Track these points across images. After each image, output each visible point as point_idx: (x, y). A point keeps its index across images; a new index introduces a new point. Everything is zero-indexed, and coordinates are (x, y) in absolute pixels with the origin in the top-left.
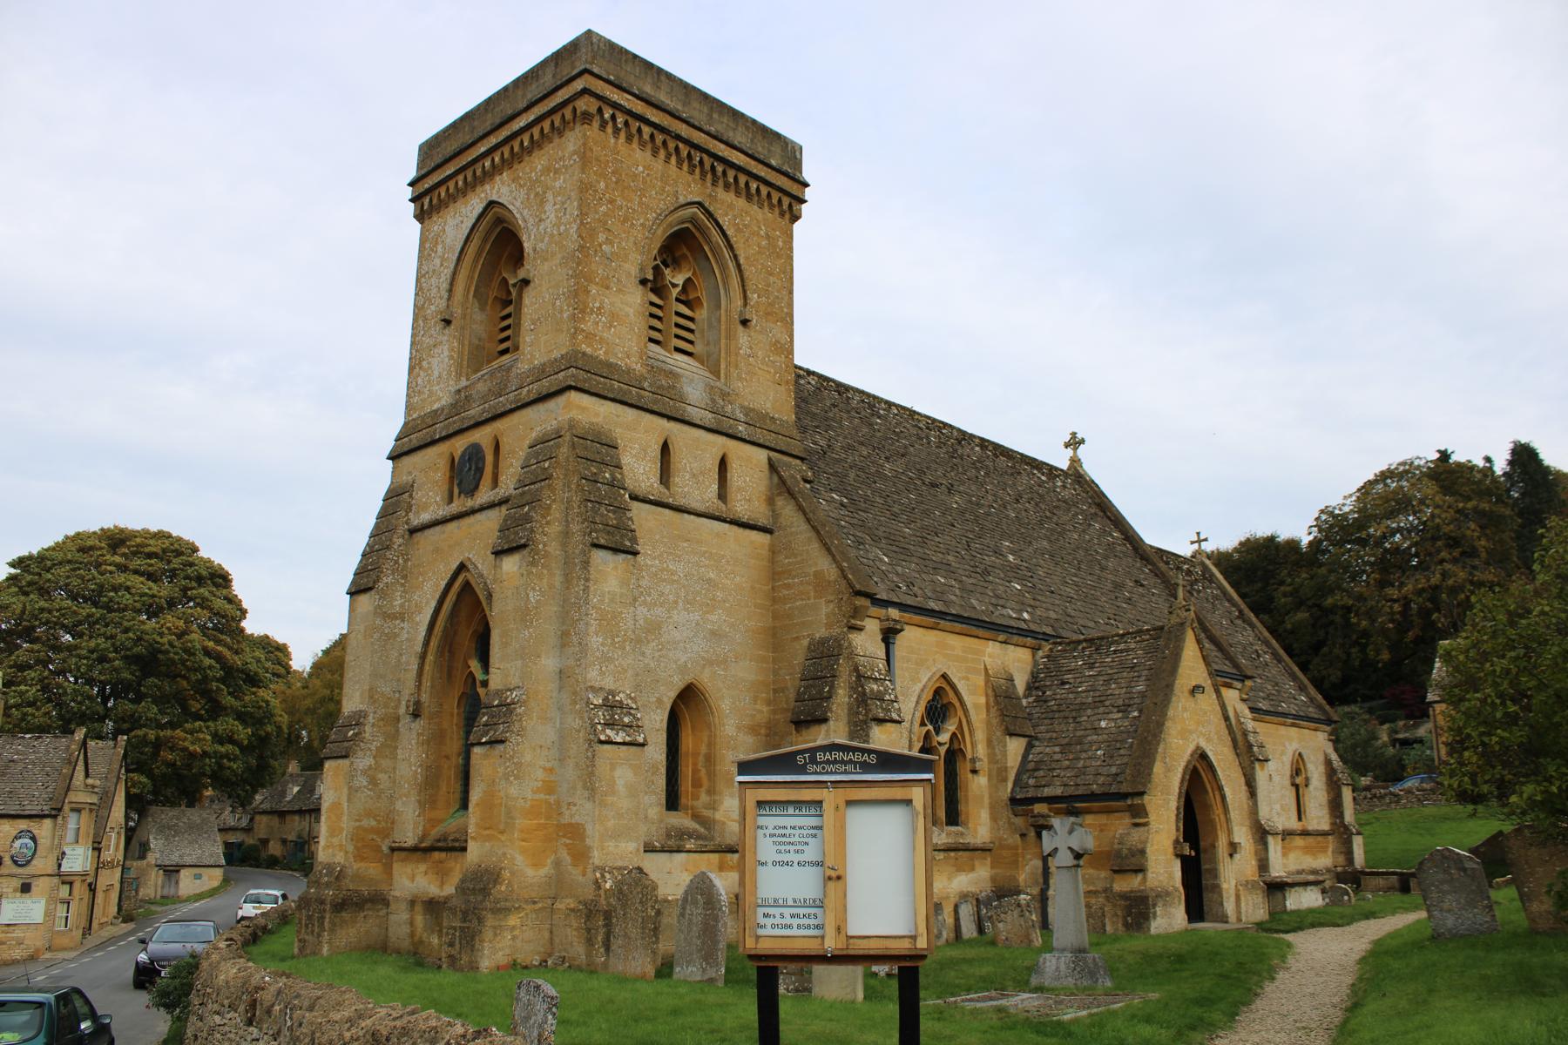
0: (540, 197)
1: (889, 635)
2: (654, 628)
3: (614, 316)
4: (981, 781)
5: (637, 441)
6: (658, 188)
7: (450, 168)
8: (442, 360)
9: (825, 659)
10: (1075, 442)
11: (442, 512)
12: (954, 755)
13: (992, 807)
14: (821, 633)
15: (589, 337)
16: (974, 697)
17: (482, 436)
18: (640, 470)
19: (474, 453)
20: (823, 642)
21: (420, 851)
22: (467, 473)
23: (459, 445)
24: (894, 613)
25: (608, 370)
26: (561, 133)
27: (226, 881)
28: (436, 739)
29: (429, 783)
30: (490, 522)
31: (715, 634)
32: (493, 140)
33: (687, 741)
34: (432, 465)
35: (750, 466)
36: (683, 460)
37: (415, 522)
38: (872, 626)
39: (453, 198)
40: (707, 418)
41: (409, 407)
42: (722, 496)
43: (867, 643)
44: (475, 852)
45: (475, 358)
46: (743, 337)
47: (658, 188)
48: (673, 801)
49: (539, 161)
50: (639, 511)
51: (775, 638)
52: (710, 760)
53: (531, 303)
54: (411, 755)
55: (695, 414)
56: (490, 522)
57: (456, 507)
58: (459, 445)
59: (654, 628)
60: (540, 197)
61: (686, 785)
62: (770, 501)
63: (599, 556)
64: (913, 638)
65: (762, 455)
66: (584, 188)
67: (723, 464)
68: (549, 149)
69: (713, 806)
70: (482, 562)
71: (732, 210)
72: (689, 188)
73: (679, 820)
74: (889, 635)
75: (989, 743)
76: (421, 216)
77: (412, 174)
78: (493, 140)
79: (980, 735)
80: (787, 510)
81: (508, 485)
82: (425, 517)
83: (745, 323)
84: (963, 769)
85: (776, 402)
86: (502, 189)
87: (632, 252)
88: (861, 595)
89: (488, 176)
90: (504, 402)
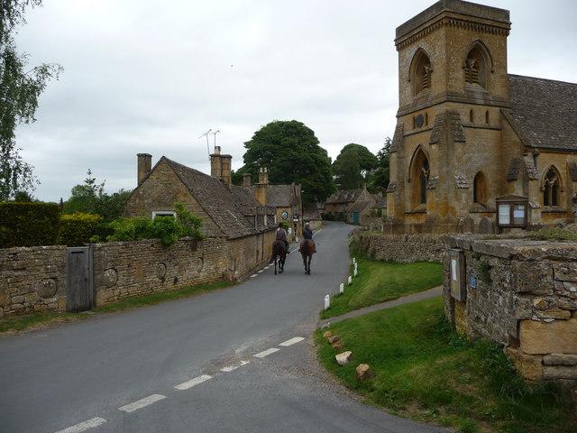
0: (436, 47)
1: (535, 156)
2: (470, 159)
3: (456, 79)
4: (565, 194)
5: (463, 111)
6: (466, 38)
7: (407, 35)
8: (409, 91)
9: (517, 163)
10: (44, 71)
11: (412, 132)
12: (556, 186)
13: (568, 200)
14: (515, 157)
15: (450, 86)
16: (562, 170)
17: (423, 112)
18: (465, 119)
19: (420, 116)
20: (516, 159)
21: (412, 214)
22: (419, 122)
23: (416, 115)
24: (537, 150)
25: (456, 94)
26: (438, 28)
27: (323, 224)
28: (414, 187)
29: (413, 198)
30: (428, 134)
31: (486, 159)
32: (419, 30)
33: (479, 186)
34: (408, 120)
35: (494, 113)
36: (477, 114)
37: (406, 134)
38: (530, 154)
39: (407, 45)
40: (482, 102)
41: (400, 104)
42: (487, 122)
43: (528, 160)
44: (428, 213)
45: (416, 91)
46: (492, 76)
47: (466, 38)
48: (475, 201)
49: (432, 37)
50: (467, 131)
51: (501, 158)
52: (485, 190)
53: (433, 77)
54: (408, 192)
55: (478, 102)
56: (428, 134)
57: (415, 131)
58: (416, 115)
59: (470, 159)
60: (436, 47)
61: (479, 197)
62: (500, 121)
63: (456, 144)
64: (542, 156)
65: (498, 109)
66: (447, 45)
67: (487, 113)
68: (436, 33)
69: (486, 202)
70: (426, 146)
71: (488, 39)
72: (475, 37)
73: (477, 205)
74: (535, 156)
75: (567, 183)
76: (398, 50)
77: (395, 37)
78: (419, 30)
79: (564, 182)
80: (506, 124)
81: (431, 125)
82: (408, 133)
83: (492, 72)
84: (559, 192)
85: (498, 91)
86: (423, 44)
87: (459, 60)
88: (527, 148)
89: (417, 40)
90: (428, 104)
